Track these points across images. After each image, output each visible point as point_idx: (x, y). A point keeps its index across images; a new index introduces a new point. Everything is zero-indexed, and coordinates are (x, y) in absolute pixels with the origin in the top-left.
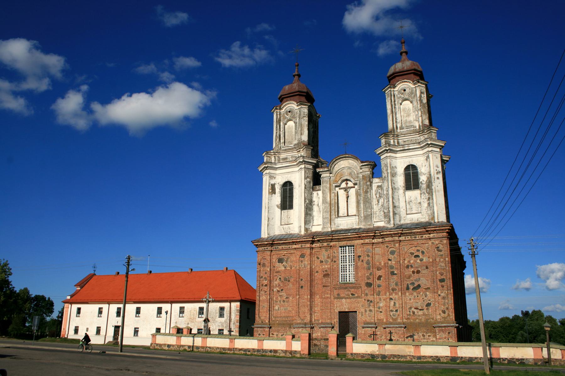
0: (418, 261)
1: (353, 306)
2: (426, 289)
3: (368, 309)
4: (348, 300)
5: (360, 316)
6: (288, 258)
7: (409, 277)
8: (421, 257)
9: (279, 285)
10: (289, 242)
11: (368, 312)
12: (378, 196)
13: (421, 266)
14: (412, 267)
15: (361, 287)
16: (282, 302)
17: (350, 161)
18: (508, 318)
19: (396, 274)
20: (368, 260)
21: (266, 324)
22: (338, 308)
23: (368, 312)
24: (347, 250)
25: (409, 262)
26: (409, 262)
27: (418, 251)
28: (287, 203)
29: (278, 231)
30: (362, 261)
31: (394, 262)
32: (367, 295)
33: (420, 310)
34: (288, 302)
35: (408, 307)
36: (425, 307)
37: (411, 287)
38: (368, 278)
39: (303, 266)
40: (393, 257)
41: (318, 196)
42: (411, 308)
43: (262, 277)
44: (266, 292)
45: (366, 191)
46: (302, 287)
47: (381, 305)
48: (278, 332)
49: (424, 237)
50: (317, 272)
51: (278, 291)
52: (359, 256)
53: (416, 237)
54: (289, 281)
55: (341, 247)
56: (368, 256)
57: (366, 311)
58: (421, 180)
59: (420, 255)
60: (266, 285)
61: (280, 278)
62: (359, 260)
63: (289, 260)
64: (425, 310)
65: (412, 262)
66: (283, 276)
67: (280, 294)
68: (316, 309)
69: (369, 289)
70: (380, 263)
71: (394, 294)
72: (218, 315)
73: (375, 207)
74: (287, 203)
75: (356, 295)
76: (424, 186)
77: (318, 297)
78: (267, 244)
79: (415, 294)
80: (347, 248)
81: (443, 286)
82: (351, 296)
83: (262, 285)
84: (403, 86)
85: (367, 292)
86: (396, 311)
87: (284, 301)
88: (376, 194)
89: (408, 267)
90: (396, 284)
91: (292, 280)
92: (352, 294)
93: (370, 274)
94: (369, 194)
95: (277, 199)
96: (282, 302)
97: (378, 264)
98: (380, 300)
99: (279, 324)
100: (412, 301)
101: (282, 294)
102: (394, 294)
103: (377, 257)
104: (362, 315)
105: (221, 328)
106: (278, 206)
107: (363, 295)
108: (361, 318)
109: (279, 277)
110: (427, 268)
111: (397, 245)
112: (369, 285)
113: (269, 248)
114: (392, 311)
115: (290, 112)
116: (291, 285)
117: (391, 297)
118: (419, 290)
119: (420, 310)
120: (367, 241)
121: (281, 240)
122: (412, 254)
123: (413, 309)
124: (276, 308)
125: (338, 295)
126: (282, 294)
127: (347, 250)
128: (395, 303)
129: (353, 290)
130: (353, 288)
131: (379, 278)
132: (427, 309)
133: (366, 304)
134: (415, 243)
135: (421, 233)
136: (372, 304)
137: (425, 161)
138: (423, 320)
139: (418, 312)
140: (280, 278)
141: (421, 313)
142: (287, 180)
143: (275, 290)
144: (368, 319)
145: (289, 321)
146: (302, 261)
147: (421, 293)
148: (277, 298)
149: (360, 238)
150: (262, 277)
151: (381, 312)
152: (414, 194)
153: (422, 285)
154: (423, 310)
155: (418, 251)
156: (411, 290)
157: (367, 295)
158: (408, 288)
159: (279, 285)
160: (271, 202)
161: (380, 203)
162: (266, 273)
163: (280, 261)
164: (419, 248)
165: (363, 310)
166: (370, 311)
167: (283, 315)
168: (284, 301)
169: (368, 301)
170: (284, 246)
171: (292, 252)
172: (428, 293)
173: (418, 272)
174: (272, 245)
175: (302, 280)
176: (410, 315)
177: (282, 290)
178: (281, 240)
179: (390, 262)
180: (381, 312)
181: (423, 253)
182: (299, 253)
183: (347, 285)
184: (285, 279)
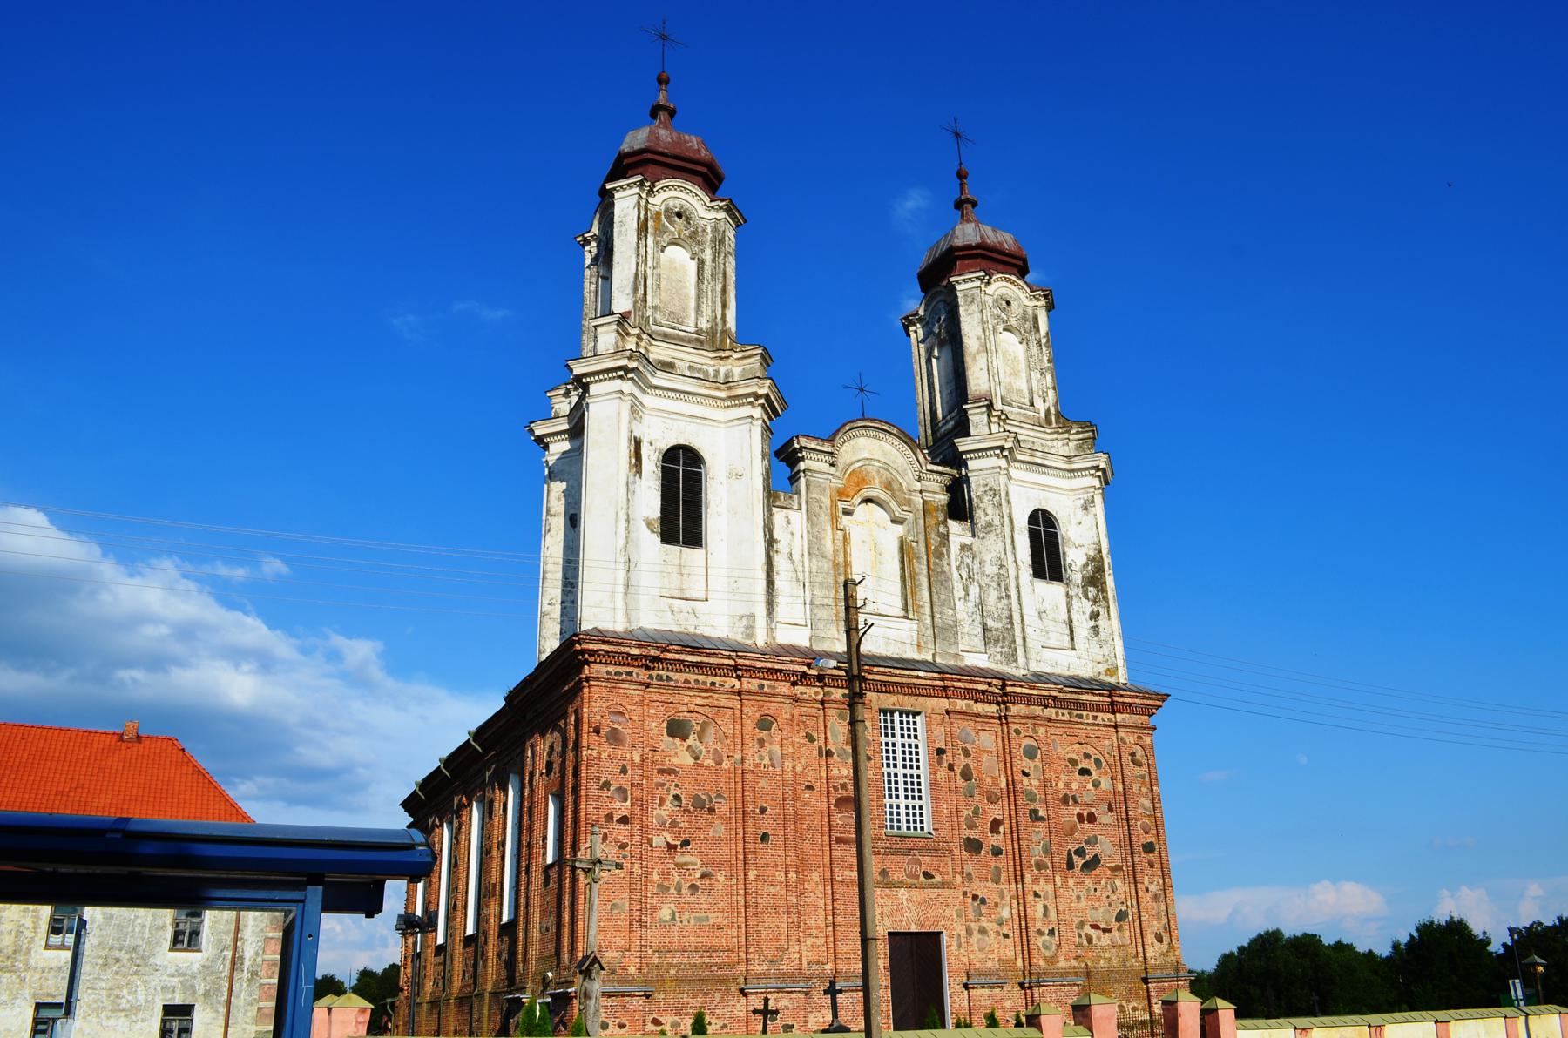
0: (1090, 786)
1: (932, 913)
2: (1113, 869)
3: (975, 926)
4: (915, 893)
5: (954, 947)
6: (704, 726)
7: (1072, 830)
8: (1095, 775)
9: (674, 824)
10: (720, 666)
11: (976, 936)
12: (965, 576)
13: (1096, 803)
14: (1075, 802)
15: (951, 852)
16: (685, 891)
17: (888, 447)
18: (1232, 953)
19: (1042, 819)
20: (967, 766)
21: (632, 981)
22: (887, 922)
23: (976, 936)
24: (897, 725)
25: (1068, 785)
26: (1068, 785)
27: (1087, 756)
28: (682, 519)
29: (654, 617)
30: (951, 767)
31: (1036, 783)
32: (969, 877)
33: (1105, 930)
34: (710, 891)
35: (1077, 921)
36: (1115, 925)
37: (1078, 862)
38: (972, 826)
39: (766, 761)
40: (1032, 764)
41: (792, 525)
42: (1081, 925)
43: (607, 785)
44: (623, 846)
45: (936, 550)
46: (765, 837)
47: (1006, 913)
48: (678, 1012)
49: (1099, 721)
50: (810, 787)
51: (671, 847)
52: (940, 752)
53: (1095, 718)
54: (712, 810)
55: (885, 712)
56: (966, 753)
57: (969, 932)
58: (1068, 561)
59: (1093, 769)
60: (624, 820)
61: (677, 797)
62: (940, 763)
63: (711, 730)
64: (1115, 932)
65: (1075, 786)
66: (688, 789)
67: (680, 859)
68: (811, 921)
69: (975, 859)
70: (995, 781)
71: (1042, 881)
72: (169, 934)
73: (959, 604)
74: (682, 519)
75: (938, 878)
76: (1077, 578)
77: (816, 876)
78: (635, 658)
79: (1089, 883)
80: (897, 715)
81: (1151, 865)
82: (922, 878)
83: (609, 817)
84: (1004, 291)
85: (969, 868)
86: (1052, 932)
87: (693, 887)
88: (958, 568)
89: (1065, 800)
90: (1048, 851)
91: (723, 808)
92: (927, 875)
93: (975, 812)
94: (945, 562)
95: (649, 500)
96: (685, 891)
97: (989, 781)
98: (1002, 896)
99: (679, 980)
100: (1083, 903)
101: (687, 859)
102: (1042, 881)
103: (985, 757)
104: (960, 946)
105: (178, 1000)
106: (649, 524)
107: (959, 879)
108: (953, 957)
109: (674, 791)
110: (1110, 809)
111: (1042, 730)
112: (973, 846)
113: (643, 675)
114: (1040, 933)
115: (679, 215)
116: (718, 829)
117: (1036, 888)
118: (1097, 872)
119: (1105, 930)
120: (961, 704)
121: (695, 650)
122: (1074, 762)
123: (1087, 929)
124: (665, 913)
125: (884, 873)
126: (687, 859)
127: (897, 725)
128: (1045, 907)
129: (927, 859)
130: (929, 851)
131: (995, 826)
132: (1120, 929)
133: (970, 909)
134: (1077, 730)
135: (1098, 708)
136: (984, 909)
137: (1080, 512)
138: (1115, 962)
139: (1099, 938)
140: (677, 797)
141: (1105, 940)
142: (682, 442)
143: (658, 841)
144: (978, 959)
145: (720, 966)
146: (761, 742)
147: (1103, 882)
148: (666, 875)
149: (945, 692)
150: (607, 785)
151: (1006, 936)
152: (1051, 592)
153: (1103, 858)
154: (1109, 931)
155: (1087, 756)
156: (1077, 870)
157: (969, 877)
158: (1070, 865)
159: (674, 824)
160: (620, 498)
161: (971, 597)
162: (624, 771)
163: (677, 729)
164: (1089, 750)
165: (960, 929)
166: (983, 931)
167: (692, 942)
168: (693, 887)
169: (975, 898)
170: (692, 677)
171: (723, 703)
172: (1118, 883)
173: (1092, 818)
174: (650, 662)
175: (763, 810)
176: (1081, 945)
177: (686, 843)
178: (695, 650)
179: (1025, 781)
180: (1006, 936)
181: (1097, 761)
182: (752, 712)
183: (909, 843)
184: (698, 803)
